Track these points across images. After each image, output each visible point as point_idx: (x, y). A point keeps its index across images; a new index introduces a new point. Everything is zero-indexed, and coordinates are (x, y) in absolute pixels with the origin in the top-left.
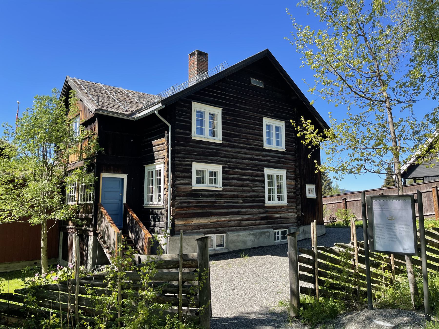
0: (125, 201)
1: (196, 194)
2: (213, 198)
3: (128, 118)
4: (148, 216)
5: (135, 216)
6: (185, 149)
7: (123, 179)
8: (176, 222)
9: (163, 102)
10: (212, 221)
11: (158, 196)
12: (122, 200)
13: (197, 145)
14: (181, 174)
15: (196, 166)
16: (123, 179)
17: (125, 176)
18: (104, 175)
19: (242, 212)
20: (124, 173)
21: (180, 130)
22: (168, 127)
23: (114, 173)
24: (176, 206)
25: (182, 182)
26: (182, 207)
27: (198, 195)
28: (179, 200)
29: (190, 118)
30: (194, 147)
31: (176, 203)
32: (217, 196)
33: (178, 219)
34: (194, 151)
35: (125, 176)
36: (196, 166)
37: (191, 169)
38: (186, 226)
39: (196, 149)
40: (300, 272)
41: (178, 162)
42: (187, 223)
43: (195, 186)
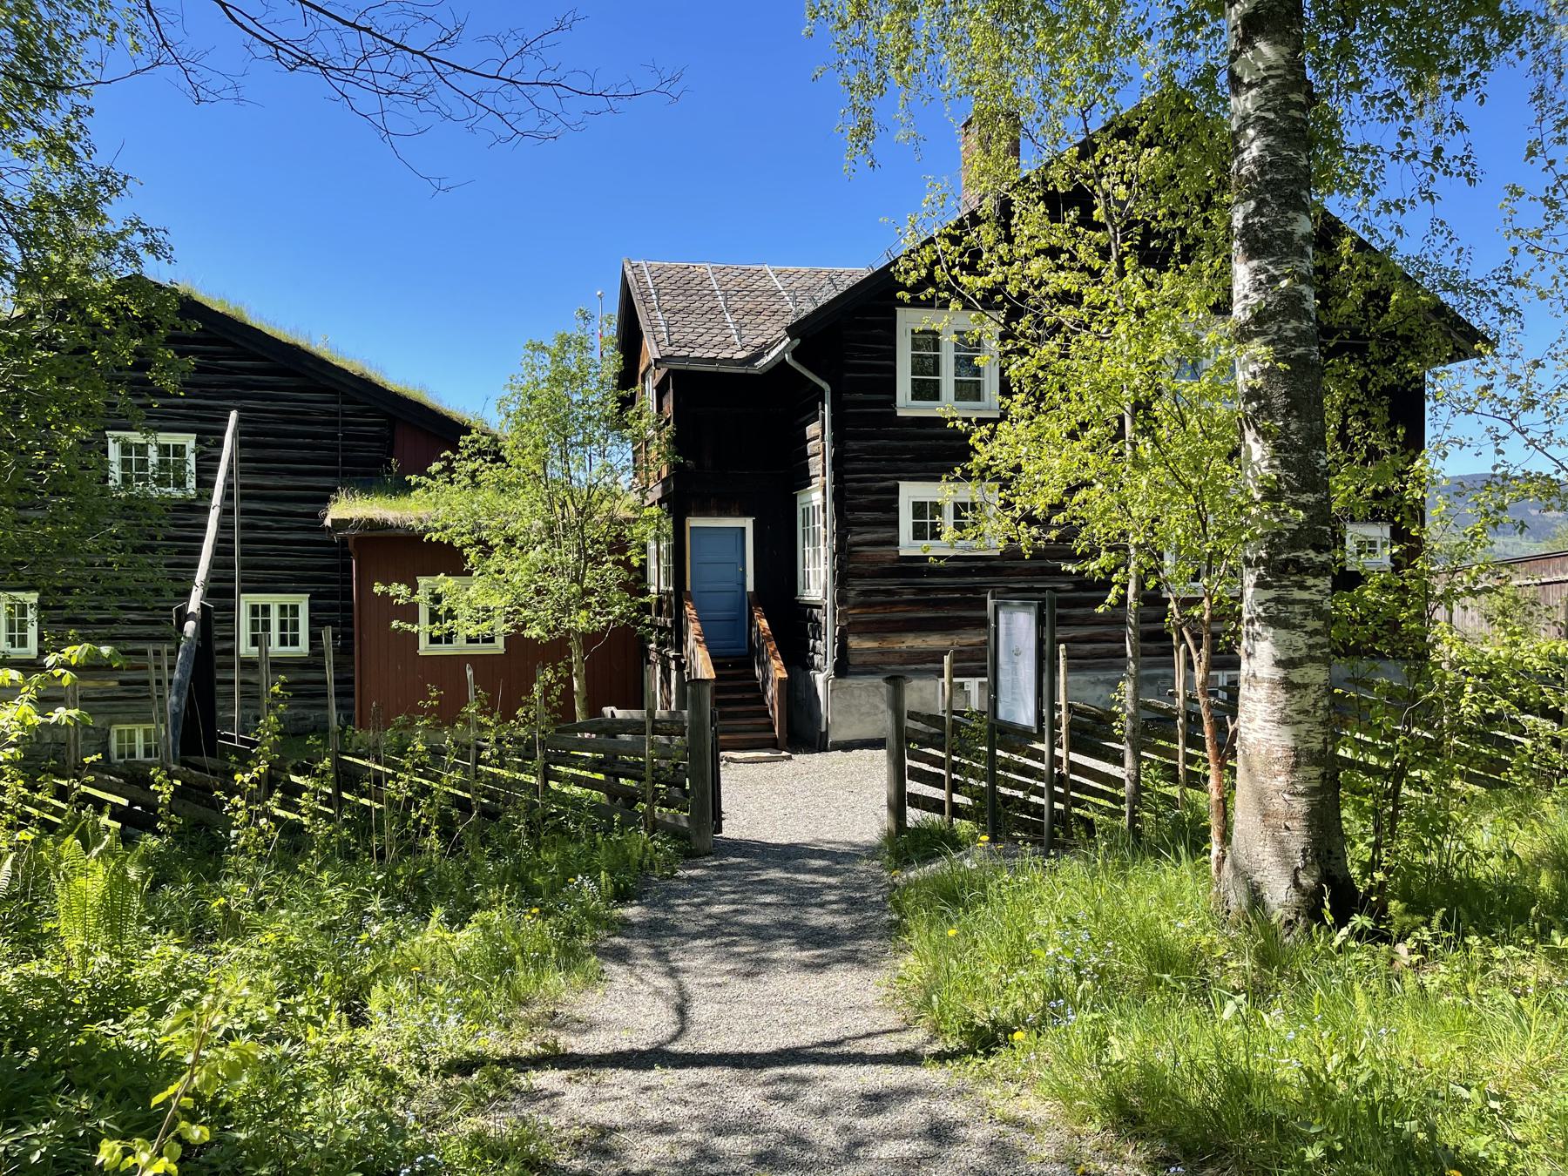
0: (750, 587)
1: (915, 567)
2: (969, 580)
3: (741, 370)
4: (794, 626)
5: (764, 623)
6: (873, 447)
7: (743, 529)
8: (854, 642)
9: (792, 330)
10: (965, 642)
11: (816, 578)
12: (744, 585)
13: (915, 430)
14: (866, 516)
15: (910, 493)
16: (743, 529)
17: (748, 523)
18: (693, 522)
19: (1072, 617)
20: (745, 514)
21: (860, 396)
22: (822, 391)
23: (719, 515)
24: (851, 601)
25: (868, 537)
26: (871, 605)
27: (918, 572)
28: (859, 585)
29: (892, 356)
30: (904, 437)
31: (852, 593)
32: (980, 572)
33: (859, 634)
34: (906, 450)
35: (748, 523)
36: (910, 493)
37: (897, 501)
38: (883, 654)
39: (911, 444)
40: (908, 762)
41: (855, 484)
42: (886, 645)
43: (908, 546)
